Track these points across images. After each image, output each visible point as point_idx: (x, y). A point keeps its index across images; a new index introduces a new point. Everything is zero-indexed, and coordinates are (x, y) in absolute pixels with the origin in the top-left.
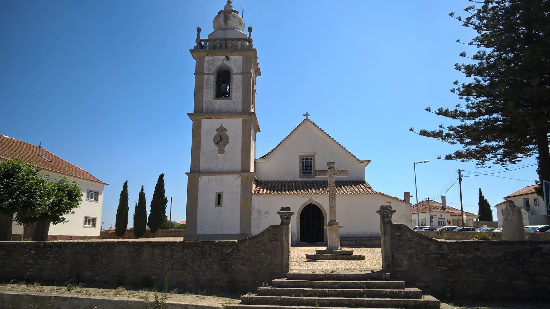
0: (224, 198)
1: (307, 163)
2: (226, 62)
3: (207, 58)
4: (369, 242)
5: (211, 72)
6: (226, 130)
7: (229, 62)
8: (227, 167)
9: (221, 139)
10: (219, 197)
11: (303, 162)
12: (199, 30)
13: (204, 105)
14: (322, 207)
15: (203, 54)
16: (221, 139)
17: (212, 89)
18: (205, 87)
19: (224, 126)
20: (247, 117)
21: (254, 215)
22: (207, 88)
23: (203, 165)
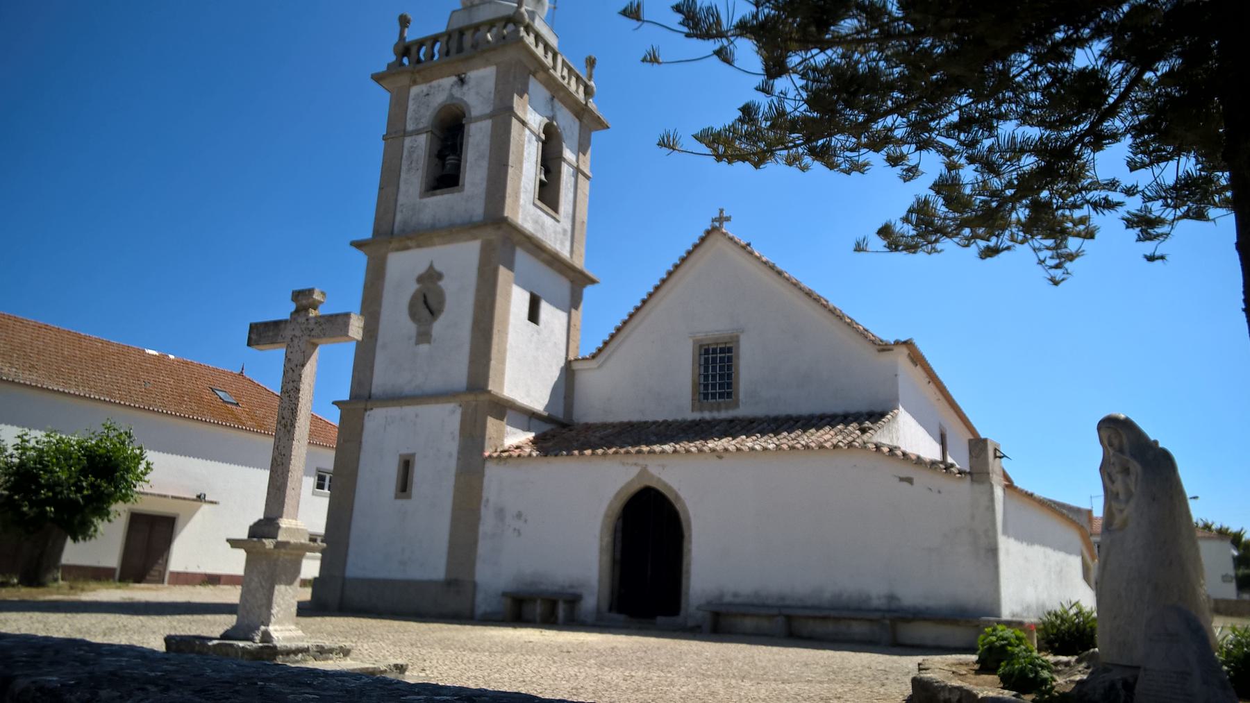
0: (419, 472)
1: (716, 366)
2: (457, 92)
3: (415, 90)
4: (830, 627)
5: (421, 126)
6: (440, 276)
7: (465, 88)
8: (435, 381)
9: (427, 304)
10: (406, 466)
11: (706, 360)
12: (404, 22)
13: (399, 217)
14: (677, 496)
15: (404, 80)
16: (427, 304)
17: (420, 173)
18: (404, 168)
19: (438, 267)
20: (492, 234)
21: (487, 524)
22: (409, 170)
23: (381, 379)
